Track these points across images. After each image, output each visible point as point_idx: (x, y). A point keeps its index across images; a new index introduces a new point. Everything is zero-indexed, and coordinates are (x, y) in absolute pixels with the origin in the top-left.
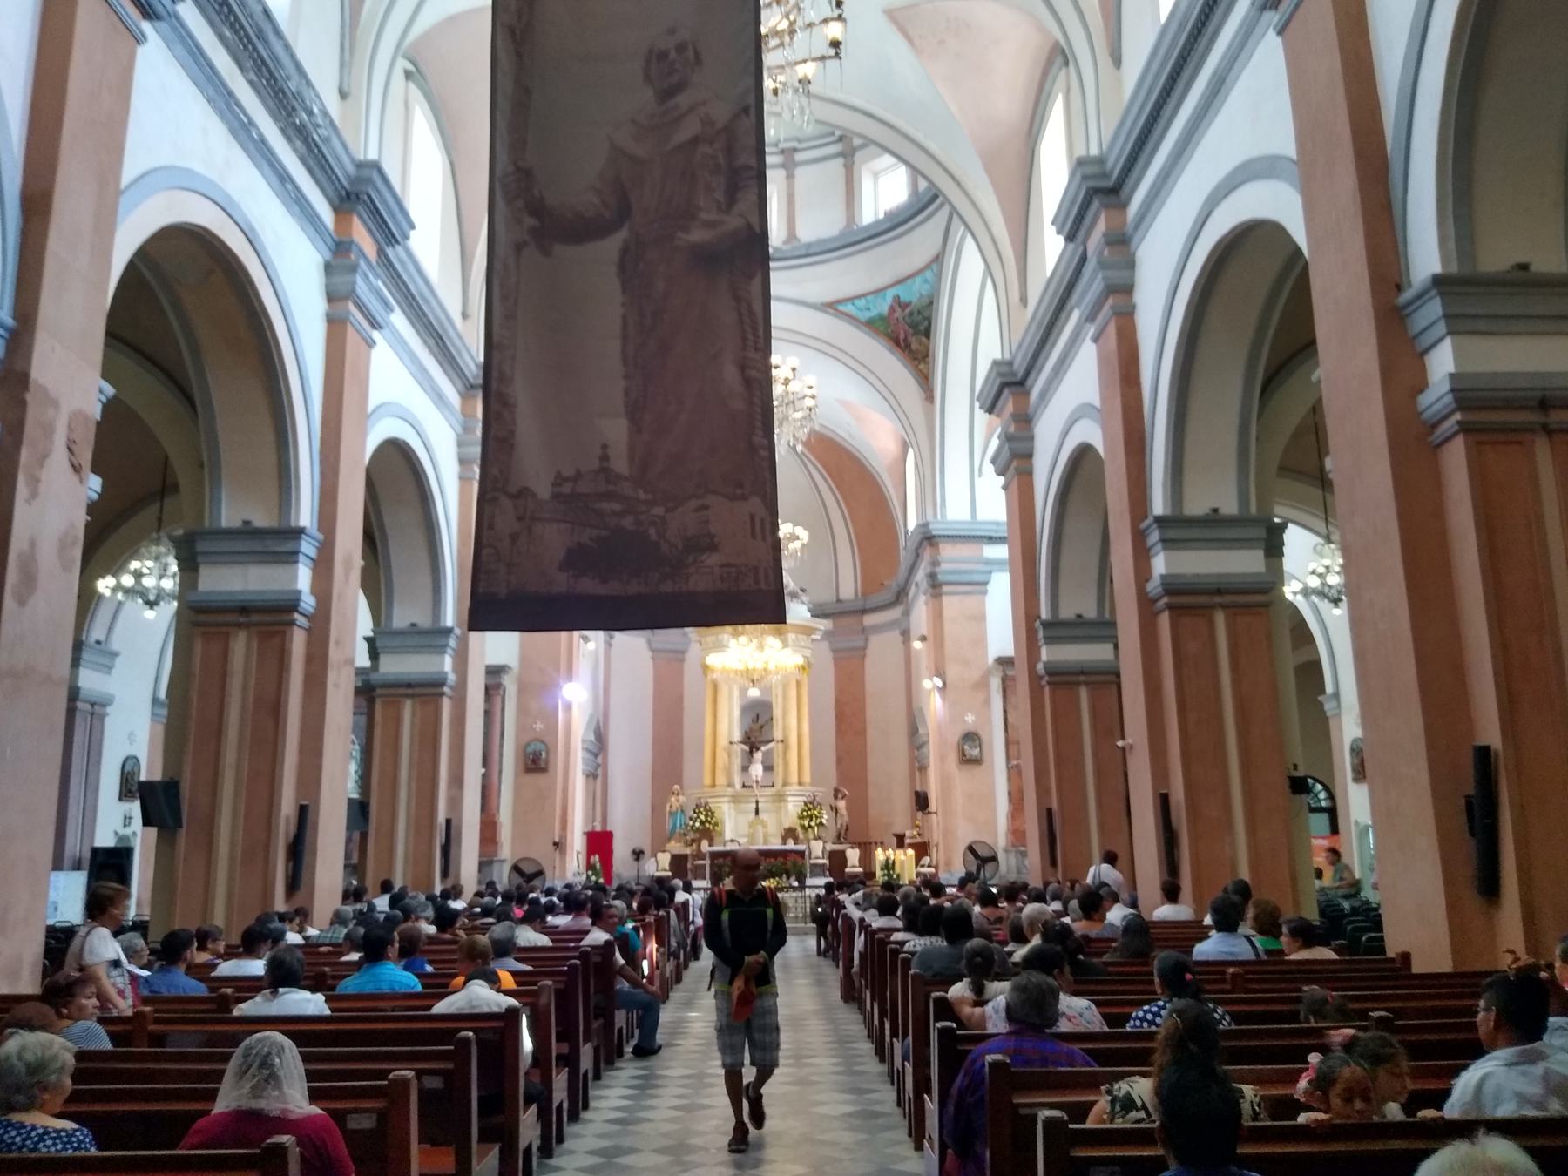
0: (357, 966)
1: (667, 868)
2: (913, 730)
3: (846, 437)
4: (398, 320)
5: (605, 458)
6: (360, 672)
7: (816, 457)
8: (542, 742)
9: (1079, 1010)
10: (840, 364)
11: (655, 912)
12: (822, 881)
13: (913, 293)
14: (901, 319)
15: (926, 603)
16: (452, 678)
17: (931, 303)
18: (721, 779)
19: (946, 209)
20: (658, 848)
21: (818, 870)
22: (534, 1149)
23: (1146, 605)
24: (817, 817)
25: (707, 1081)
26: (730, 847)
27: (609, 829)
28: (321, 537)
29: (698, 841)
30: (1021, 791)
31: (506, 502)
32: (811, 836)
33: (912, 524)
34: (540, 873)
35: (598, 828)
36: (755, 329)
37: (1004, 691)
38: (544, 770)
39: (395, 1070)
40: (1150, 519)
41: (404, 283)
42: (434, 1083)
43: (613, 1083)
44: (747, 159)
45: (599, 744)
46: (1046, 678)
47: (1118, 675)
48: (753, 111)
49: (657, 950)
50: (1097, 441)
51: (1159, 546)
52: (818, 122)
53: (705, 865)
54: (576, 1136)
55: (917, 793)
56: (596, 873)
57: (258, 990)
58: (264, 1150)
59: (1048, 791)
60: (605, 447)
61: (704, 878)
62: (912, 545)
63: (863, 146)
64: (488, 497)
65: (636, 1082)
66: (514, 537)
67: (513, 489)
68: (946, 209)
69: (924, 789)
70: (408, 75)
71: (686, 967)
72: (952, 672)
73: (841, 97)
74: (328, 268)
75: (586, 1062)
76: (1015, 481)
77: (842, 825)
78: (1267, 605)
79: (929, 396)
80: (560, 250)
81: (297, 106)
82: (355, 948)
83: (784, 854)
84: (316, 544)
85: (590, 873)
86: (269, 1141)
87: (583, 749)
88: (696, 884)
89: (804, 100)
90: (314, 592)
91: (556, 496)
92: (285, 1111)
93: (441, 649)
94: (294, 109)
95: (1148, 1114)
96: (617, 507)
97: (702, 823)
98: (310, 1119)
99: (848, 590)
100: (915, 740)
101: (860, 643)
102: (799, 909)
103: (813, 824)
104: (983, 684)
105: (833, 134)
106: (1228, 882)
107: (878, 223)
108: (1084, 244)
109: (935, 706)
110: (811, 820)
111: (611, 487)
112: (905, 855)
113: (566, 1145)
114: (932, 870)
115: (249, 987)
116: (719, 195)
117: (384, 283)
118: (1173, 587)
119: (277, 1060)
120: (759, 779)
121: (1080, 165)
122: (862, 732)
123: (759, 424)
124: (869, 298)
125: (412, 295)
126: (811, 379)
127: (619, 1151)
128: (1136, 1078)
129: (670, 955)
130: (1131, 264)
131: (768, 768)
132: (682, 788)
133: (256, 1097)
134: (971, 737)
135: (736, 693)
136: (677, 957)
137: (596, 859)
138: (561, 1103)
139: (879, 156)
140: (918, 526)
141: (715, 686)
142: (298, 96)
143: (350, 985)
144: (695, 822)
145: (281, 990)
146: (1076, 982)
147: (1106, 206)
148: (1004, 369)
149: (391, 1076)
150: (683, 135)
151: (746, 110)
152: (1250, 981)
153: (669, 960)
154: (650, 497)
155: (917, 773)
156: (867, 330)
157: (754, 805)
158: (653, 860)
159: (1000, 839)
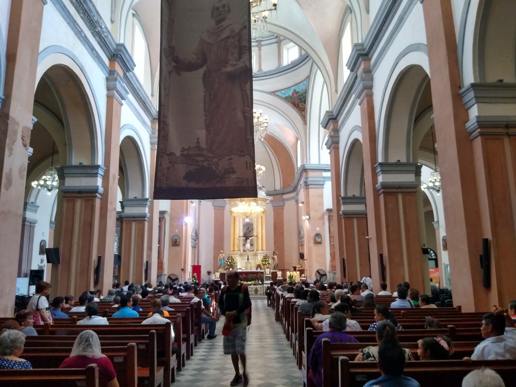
1: (219, 277)
2: (299, 233)
3: (277, 136)
4: (130, 96)
5: (198, 142)
6: (118, 213)
7: (268, 143)
8: (178, 236)
9: (353, 324)
11: (215, 292)
12: (269, 282)
13: (300, 88)
14: (296, 97)
15: (304, 191)
16: (148, 215)
17: (306, 92)
18: (236, 249)
19: (311, 61)
20: (216, 271)
21: (268, 278)
22: (175, 368)
23: (376, 192)
24: (268, 261)
27: (199, 265)
28: (105, 168)
31: (166, 157)
32: (266, 267)
33: (299, 165)
34: (177, 279)
35: (196, 264)
36: (248, 100)
37: (329, 220)
38: (178, 245)
40: (377, 164)
41: (133, 85)
42: (142, 347)
45: (196, 237)
46: (343, 216)
47: (366, 215)
48: (247, 27)
49: (215, 304)
51: (380, 173)
54: (189, 364)
55: (300, 253)
56: (195, 279)
60: (198, 139)
62: (299, 172)
63: (284, 40)
64: (160, 155)
66: (168, 169)
67: (168, 153)
68: (311, 61)
69: (303, 252)
70: (134, 15)
72: (312, 213)
73: (276, 23)
74: (107, 79)
78: (415, 192)
79: (305, 123)
80: (184, 74)
83: (257, 273)
84: (104, 171)
85: (193, 279)
86: (89, 366)
87: (191, 238)
89: (265, 24)
90: (103, 187)
91: (182, 155)
92: (93, 356)
93: (145, 206)
94: (96, 26)
95: (375, 358)
96: (202, 159)
97: (230, 263)
98: (101, 359)
99: (278, 187)
100: (300, 237)
101: (282, 204)
102: (262, 291)
103: (266, 263)
104: (322, 218)
105: (274, 35)
107: (288, 65)
108: (357, 72)
109: (306, 225)
110: (266, 262)
111: (200, 152)
112: (296, 273)
113: (186, 367)
114: (305, 278)
115: (81, 316)
116: (236, 55)
117: (126, 84)
118: (385, 186)
119: (91, 339)
120: (249, 248)
121: (355, 46)
123: (249, 132)
124: (286, 90)
125: (135, 88)
126: (266, 117)
127: (203, 369)
128: (370, 347)
130: (372, 79)
131: (252, 245)
134: (318, 235)
135: (241, 220)
137: (195, 274)
140: (301, 166)
141: (235, 218)
142: (97, 22)
143: (117, 315)
144: (228, 262)
145: (93, 316)
146: (352, 315)
147: (363, 60)
148: (330, 114)
149: (128, 345)
150: (224, 36)
151: (245, 27)
154: (213, 155)
155: (300, 247)
156: (285, 101)
157: (247, 257)
158: (214, 275)
159: (327, 268)
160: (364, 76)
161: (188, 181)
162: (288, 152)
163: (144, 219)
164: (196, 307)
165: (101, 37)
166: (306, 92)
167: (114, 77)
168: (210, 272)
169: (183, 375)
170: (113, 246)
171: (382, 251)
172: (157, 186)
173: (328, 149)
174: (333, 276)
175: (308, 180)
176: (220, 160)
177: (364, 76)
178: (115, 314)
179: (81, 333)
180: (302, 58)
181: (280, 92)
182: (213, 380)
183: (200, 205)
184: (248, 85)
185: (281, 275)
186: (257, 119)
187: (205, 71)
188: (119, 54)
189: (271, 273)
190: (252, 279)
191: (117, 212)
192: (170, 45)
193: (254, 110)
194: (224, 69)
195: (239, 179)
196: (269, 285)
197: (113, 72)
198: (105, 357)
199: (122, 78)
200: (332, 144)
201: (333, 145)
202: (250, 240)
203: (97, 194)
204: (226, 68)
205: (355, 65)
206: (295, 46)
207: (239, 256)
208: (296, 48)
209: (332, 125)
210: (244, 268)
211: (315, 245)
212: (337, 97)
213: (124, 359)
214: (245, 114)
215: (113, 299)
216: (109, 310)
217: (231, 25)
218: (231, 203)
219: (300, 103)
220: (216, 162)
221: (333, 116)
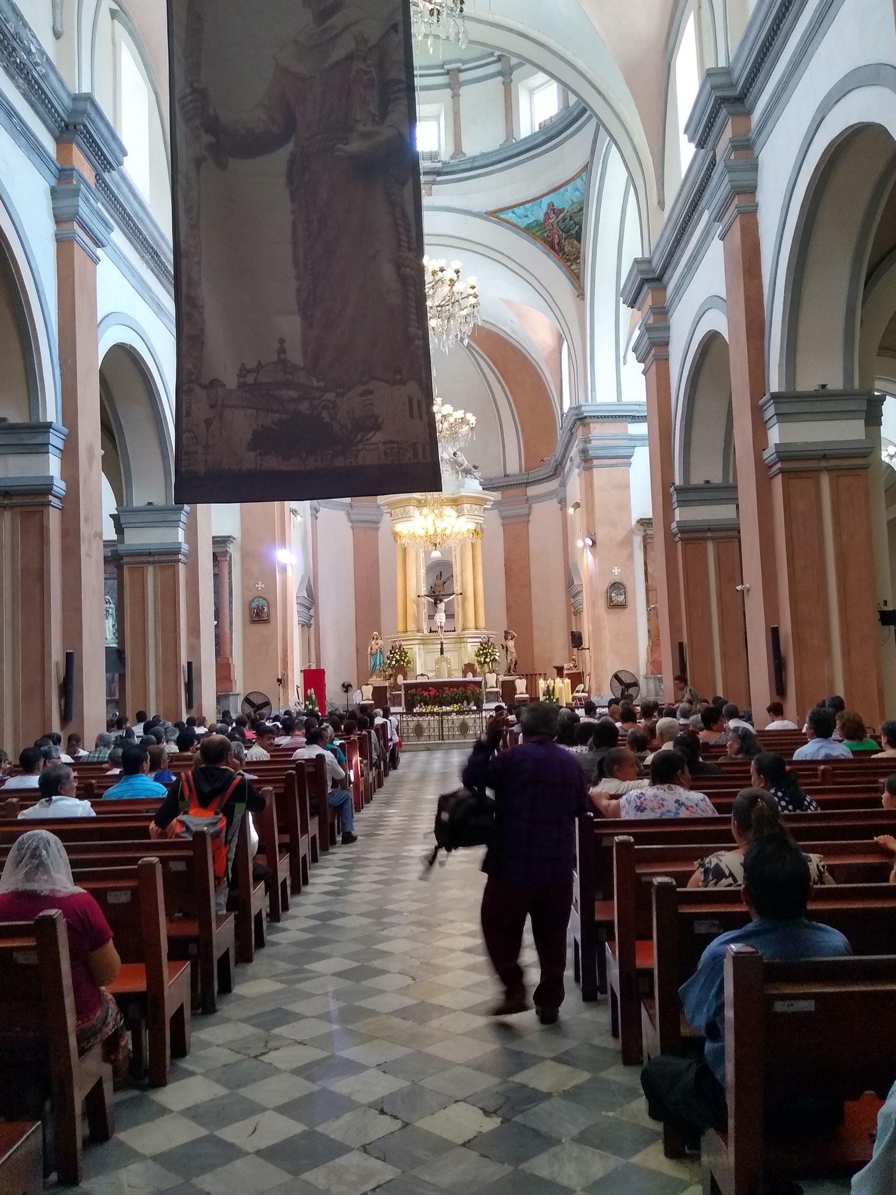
0: (116, 778)
1: (371, 698)
2: (570, 583)
3: (509, 332)
4: (118, 237)
5: (282, 351)
6: (107, 544)
7: (484, 351)
8: (264, 599)
9: (696, 802)
10: (503, 266)
11: (359, 732)
12: (493, 705)
13: (565, 200)
14: (555, 225)
15: (579, 475)
16: (185, 547)
17: (581, 209)
18: (411, 626)
19: (594, 121)
20: (363, 681)
21: (492, 697)
22: (264, 915)
23: (763, 471)
24: (491, 654)
25: (401, 861)
26: (421, 680)
27: (322, 668)
28: (66, 430)
29: (393, 676)
30: (658, 629)
31: (200, 393)
32: (487, 670)
33: (566, 407)
34: (267, 704)
35: (313, 667)
36: (408, 231)
37: (645, 547)
38: (266, 621)
39: (145, 857)
40: (768, 396)
41: (121, 206)
42: (178, 867)
43: (327, 864)
44: (395, 73)
45: (310, 601)
46: (679, 535)
47: (739, 532)
48: (401, 28)
49: (361, 762)
50: (723, 329)
51: (775, 419)
52: (471, 42)
53: (401, 694)
54: (299, 905)
55: (572, 633)
56: (312, 703)
57: (37, 799)
58: (37, 921)
59: (680, 630)
60: (282, 341)
61: (400, 705)
62: (567, 424)
63: (520, 65)
64: (185, 388)
65: (364, 863)
66: (208, 422)
67: (205, 381)
68: (594, 121)
70: (113, 14)
71: (386, 775)
72: (601, 533)
73: (491, 18)
74: (54, 192)
75: (304, 848)
76: (654, 367)
77: (511, 660)
78: (865, 468)
79: (581, 295)
80: (236, 164)
81: (18, 48)
82: (115, 765)
83: (465, 684)
84: (62, 437)
85: (307, 703)
86: (41, 914)
88: (393, 710)
89: (459, 22)
90: (63, 478)
91: (241, 385)
92: (52, 891)
94: (14, 49)
95: (735, 880)
96: (293, 394)
97: (397, 661)
98: (73, 897)
99: (514, 466)
100: (572, 591)
101: (525, 511)
102: (477, 728)
103: (488, 660)
104: (627, 542)
105: (492, 54)
106: (826, 697)
107: (533, 136)
108: (714, 149)
109: (587, 561)
110: (486, 657)
111: (289, 377)
112: (563, 683)
113: (291, 912)
114: (586, 695)
115: (28, 797)
116: (373, 108)
117: (103, 204)
118: (785, 454)
119: (44, 852)
120: (443, 625)
121: (709, 75)
122: (528, 585)
123: (413, 317)
124: (527, 206)
125: (128, 215)
126: (472, 280)
127: (332, 915)
128: (723, 852)
129: (372, 765)
130: (754, 167)
131: (450, 616)
132: (380, 634)
133: (28, 881)
134: (617, 586)
135: (422, 555)
136: (379, 767)
137: (311, 691)
138: (285, 880)
139: (533, 74)
140: (570, 409)
141: (405, 550)
142: (16, 37)
143: (113, 792)
144: (391, 661)
145: (54, 798)
146: (694, 779)
147: (733, 114)
148: (644, 267)
149: (140, 862)
150: (338, 53)
151: (395, 27)
152: (836, 775)
153: (371, 769)
154: (322, 384)
155: (573, 617)
156: (525, 235)
158: (359, 691)
159: (641, 668)
160: (732, 157)
161: (260, 454)
162: (540, 378)
163: (174, 558)
164: (312, 769)
165: (30, 77)
166: (581, 209)
167: (70, 187)
168: (350, 685)
169: (284, 930)
170: (102, 628)
171: (778, 620)
172: (183, 469)
173: (639, 362)
174: (655, 686)
175: (589, 446)
176: (342, 395)
177: (732, 157)
178: (111, 790)
179: (21, 838)
180: (570, 115)
181: (513, 213)
182: (356, 940)
183: (317, 518)
184: (408, 190)
185: (527, 688)
186: (450, 288)
187: (291, 154)
188: (80, 124)
189: (499, 684)
190: (453, 698)
191: (104, 541)
192: (196, 85)
193: (426, 260)
194: (343, 146)
195: (392, 445)
196: (493, 713)
197: (69, 172)
198: (80, 894)
199: (93, 187)
200: (651, 349)
201: (653, 351)
202: (446, 604)
203: (51, 497)
204: (347, 144)
205: (710, 129)
206: (548, 82)
207: (419, 644)
208: (553, 88)
209: (650, 294)
210: (434, 674)
211: (612, 610)
212: (661, 220)
213: (133, 895)
214: (403, 269)
215: (107, 756)
216: (98, 783)
217: (357, 22)
218: (393, 511)
219: (565, 239)
220: (329, 401)
221: (653, 271)
